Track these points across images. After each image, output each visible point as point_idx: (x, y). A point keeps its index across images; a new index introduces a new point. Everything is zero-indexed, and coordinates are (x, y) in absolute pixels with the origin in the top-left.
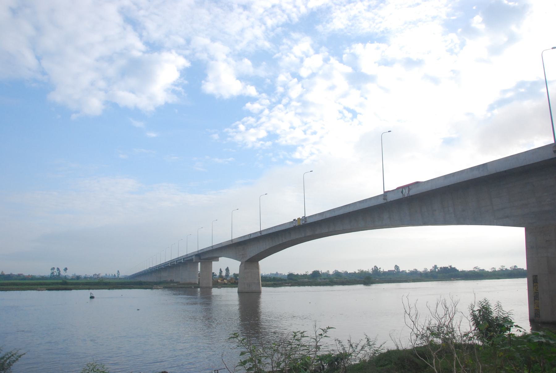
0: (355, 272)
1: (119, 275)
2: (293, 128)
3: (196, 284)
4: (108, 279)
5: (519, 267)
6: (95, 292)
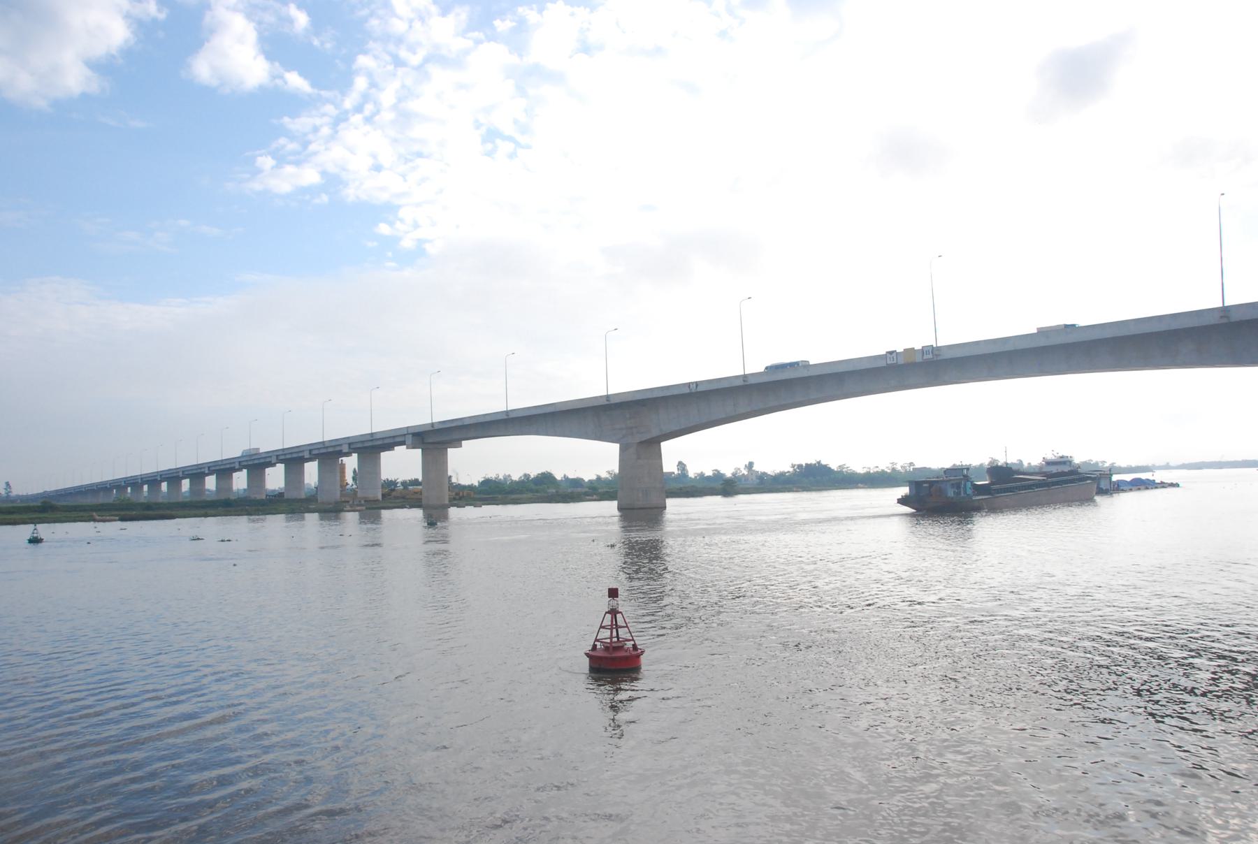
0: (599, 478)
1: (10, 492)
2: (378, 168)
3: (378, 500)
4: (22, 501)
5: (918, 465)
6: (44, 530)
